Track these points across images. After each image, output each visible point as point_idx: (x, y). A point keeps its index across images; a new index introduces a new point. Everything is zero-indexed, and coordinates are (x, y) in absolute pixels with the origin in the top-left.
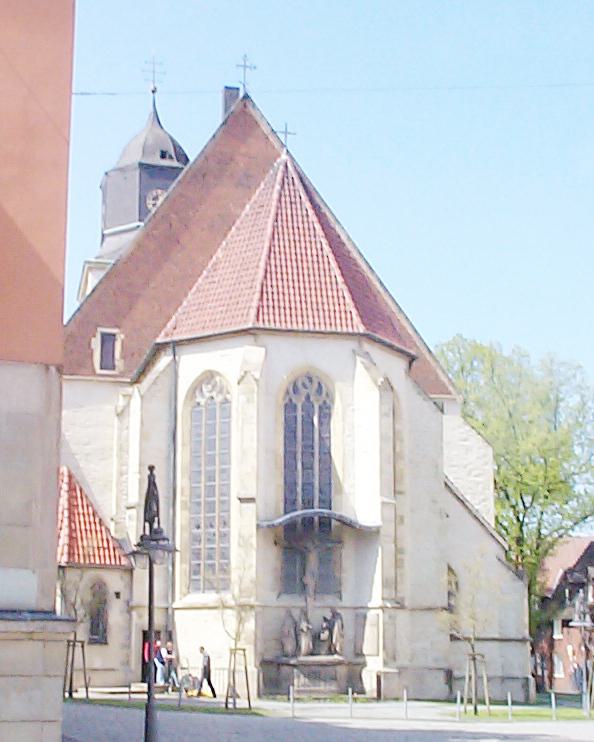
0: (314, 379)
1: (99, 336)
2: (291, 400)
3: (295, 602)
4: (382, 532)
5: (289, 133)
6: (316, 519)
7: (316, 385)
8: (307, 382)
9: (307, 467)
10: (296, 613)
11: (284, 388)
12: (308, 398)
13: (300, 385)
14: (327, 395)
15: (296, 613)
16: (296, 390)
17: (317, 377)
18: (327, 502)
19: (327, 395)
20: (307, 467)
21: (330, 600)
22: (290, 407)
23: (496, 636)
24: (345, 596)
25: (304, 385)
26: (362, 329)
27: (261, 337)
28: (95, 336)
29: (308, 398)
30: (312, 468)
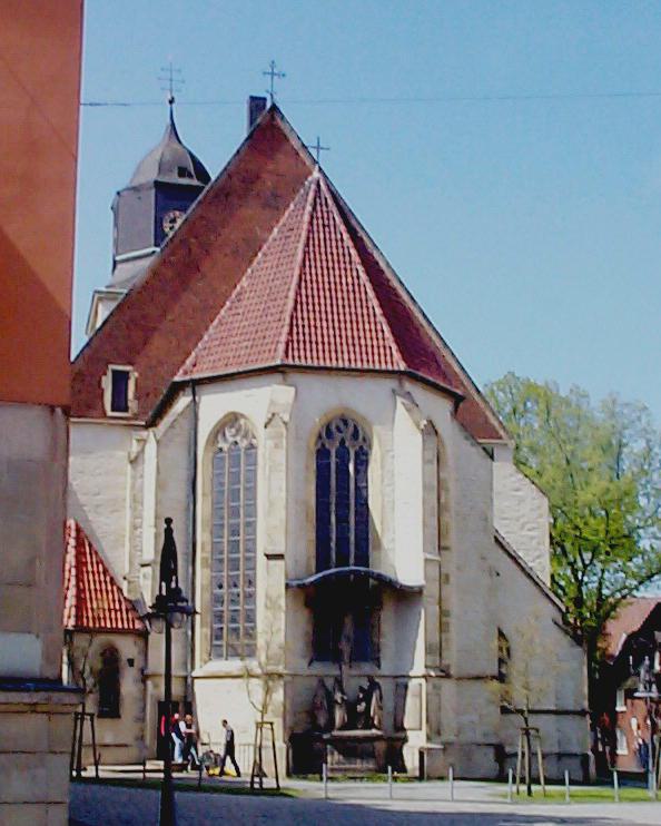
1: (110, 374)
2: (323, 445)
4: (425, 592)
7: (351, 429)
8: (342, 426)
10: (330, 683)
12: (342, 442)
13: (333, 428)
14: (364, 440)
15: (330, 683)
16: (329, 434)
17: (353, 420)
19: (364, 440)
20: (343, 520)
21: (367, 668)
22: (322, 454)
23: (553, 708)
26: (402, 366)
27: (291, 375)
29: (342, 442)
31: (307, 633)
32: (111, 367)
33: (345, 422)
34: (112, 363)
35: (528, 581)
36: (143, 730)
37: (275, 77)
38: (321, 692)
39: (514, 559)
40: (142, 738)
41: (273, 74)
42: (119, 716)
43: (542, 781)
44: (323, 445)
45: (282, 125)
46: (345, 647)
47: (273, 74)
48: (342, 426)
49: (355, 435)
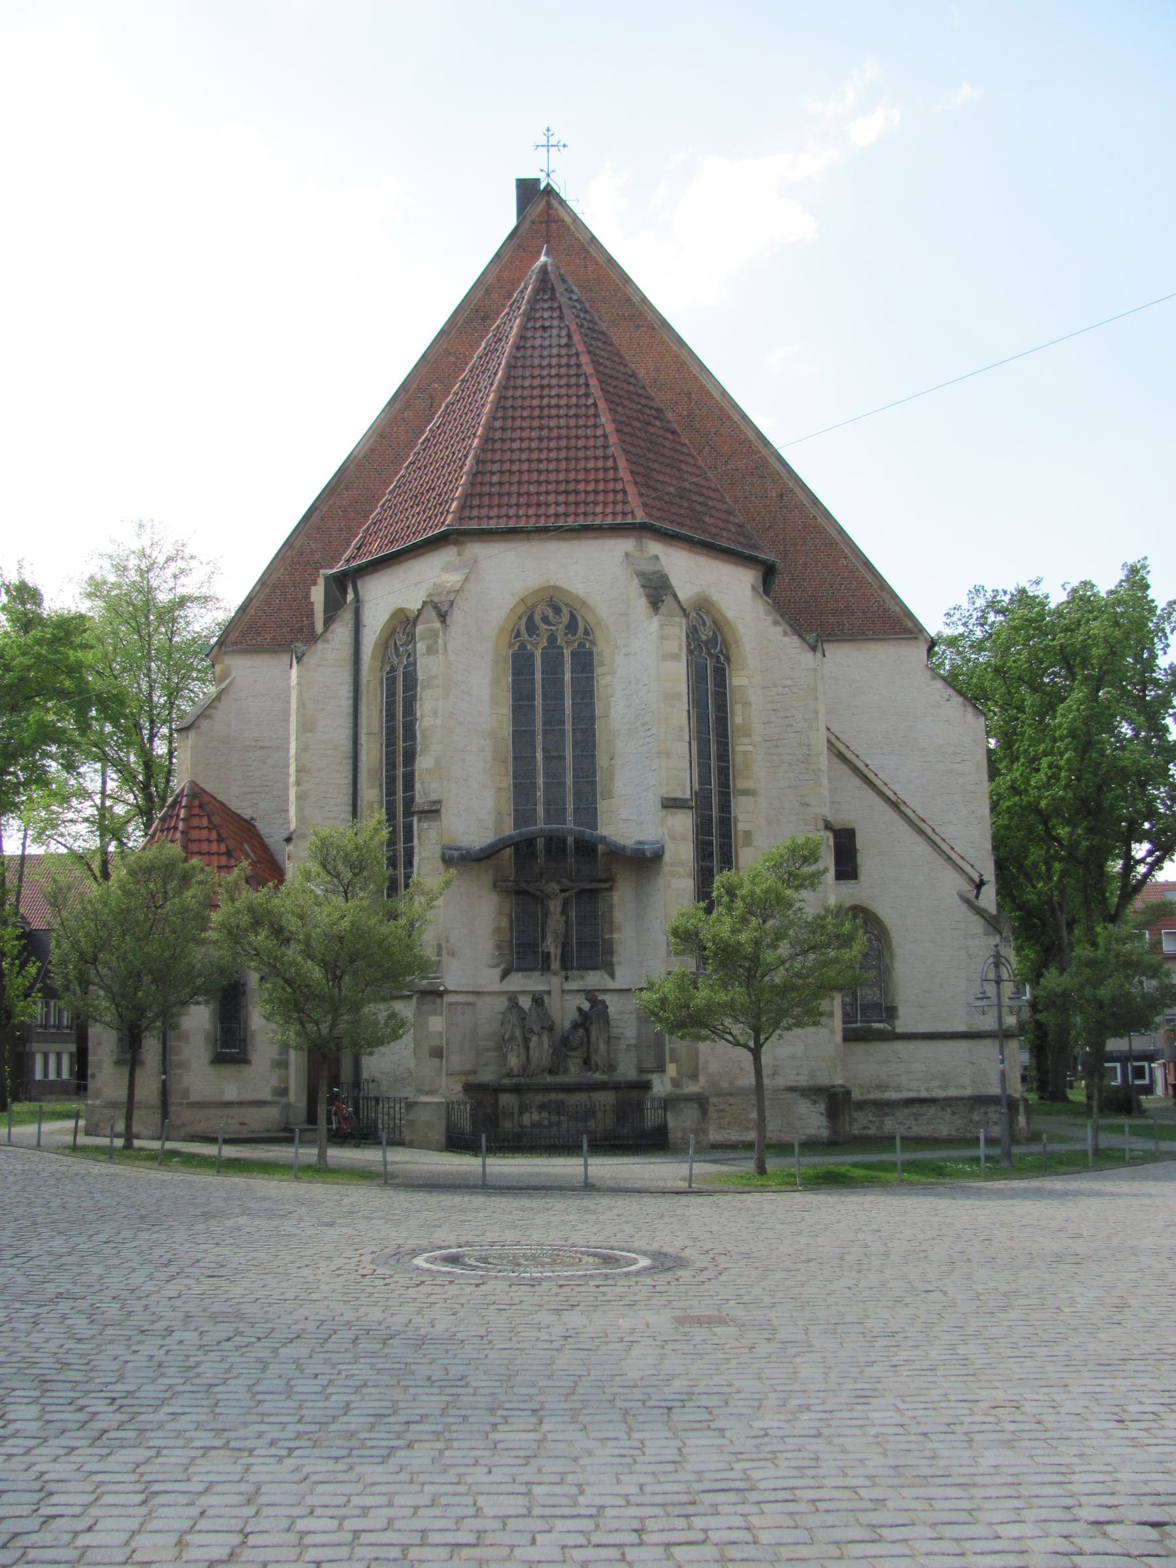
0: (565, 610)
1: (321, 581)
2: (523, 646)
3: (525, 983)
4: (667, 857)
5: (548, 226)
6: (540, 843)
7: (566, 619)
8: (551, 614)
9: (554, 757)
10: (525, 1002)
11: (734, 664)
12: (552, 638)
13: (537, 618)
14: (586, 633)
15: (525, 1002)
16: (531, 628)
17: (567, 605)
18: (588, 808)
19: (586, 633)
20: (554, 757)
21: (594, 979)
22: (521, 664)
23: (962, 1028)
24: (619, 971)
25: (546, 620)
26: (640, 517)
27: (469, 545)
28: (315, 584)
29: (552, 638)
30: (562, 758)
31: (498, 930)
32: (322, 572)
33: (557, 610)
34: (322, 567)
35: (919, 839)
36: (286, 1079)
37: (551, 149)
38: (513, 1018)
39: (895, 805)
40: (284, 1092)
41: (548, 146)
42: (245, 1061)
43: (898, 1140)
44: (523, 646)
45: (562, 213)
46: (551, 946)
47: (548, 146)
48: (551, 614)
49: (572, 627)
